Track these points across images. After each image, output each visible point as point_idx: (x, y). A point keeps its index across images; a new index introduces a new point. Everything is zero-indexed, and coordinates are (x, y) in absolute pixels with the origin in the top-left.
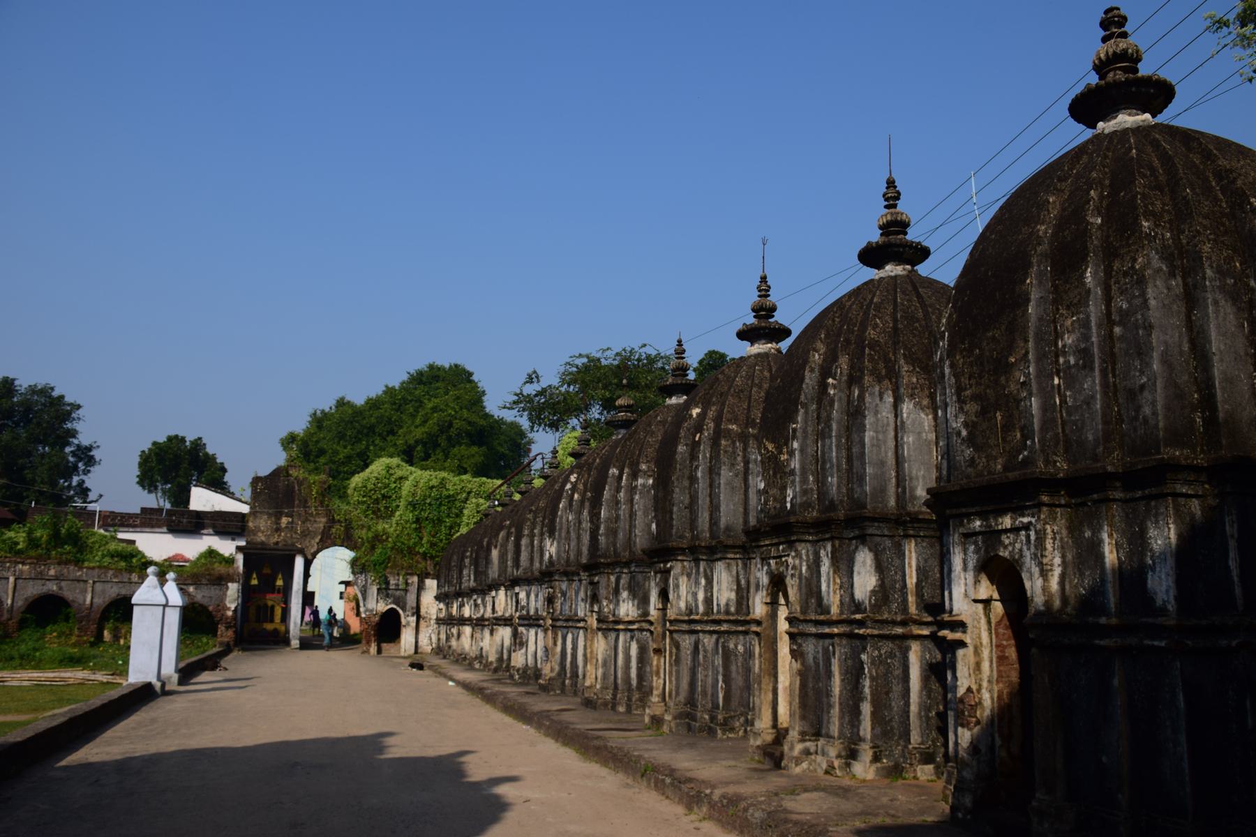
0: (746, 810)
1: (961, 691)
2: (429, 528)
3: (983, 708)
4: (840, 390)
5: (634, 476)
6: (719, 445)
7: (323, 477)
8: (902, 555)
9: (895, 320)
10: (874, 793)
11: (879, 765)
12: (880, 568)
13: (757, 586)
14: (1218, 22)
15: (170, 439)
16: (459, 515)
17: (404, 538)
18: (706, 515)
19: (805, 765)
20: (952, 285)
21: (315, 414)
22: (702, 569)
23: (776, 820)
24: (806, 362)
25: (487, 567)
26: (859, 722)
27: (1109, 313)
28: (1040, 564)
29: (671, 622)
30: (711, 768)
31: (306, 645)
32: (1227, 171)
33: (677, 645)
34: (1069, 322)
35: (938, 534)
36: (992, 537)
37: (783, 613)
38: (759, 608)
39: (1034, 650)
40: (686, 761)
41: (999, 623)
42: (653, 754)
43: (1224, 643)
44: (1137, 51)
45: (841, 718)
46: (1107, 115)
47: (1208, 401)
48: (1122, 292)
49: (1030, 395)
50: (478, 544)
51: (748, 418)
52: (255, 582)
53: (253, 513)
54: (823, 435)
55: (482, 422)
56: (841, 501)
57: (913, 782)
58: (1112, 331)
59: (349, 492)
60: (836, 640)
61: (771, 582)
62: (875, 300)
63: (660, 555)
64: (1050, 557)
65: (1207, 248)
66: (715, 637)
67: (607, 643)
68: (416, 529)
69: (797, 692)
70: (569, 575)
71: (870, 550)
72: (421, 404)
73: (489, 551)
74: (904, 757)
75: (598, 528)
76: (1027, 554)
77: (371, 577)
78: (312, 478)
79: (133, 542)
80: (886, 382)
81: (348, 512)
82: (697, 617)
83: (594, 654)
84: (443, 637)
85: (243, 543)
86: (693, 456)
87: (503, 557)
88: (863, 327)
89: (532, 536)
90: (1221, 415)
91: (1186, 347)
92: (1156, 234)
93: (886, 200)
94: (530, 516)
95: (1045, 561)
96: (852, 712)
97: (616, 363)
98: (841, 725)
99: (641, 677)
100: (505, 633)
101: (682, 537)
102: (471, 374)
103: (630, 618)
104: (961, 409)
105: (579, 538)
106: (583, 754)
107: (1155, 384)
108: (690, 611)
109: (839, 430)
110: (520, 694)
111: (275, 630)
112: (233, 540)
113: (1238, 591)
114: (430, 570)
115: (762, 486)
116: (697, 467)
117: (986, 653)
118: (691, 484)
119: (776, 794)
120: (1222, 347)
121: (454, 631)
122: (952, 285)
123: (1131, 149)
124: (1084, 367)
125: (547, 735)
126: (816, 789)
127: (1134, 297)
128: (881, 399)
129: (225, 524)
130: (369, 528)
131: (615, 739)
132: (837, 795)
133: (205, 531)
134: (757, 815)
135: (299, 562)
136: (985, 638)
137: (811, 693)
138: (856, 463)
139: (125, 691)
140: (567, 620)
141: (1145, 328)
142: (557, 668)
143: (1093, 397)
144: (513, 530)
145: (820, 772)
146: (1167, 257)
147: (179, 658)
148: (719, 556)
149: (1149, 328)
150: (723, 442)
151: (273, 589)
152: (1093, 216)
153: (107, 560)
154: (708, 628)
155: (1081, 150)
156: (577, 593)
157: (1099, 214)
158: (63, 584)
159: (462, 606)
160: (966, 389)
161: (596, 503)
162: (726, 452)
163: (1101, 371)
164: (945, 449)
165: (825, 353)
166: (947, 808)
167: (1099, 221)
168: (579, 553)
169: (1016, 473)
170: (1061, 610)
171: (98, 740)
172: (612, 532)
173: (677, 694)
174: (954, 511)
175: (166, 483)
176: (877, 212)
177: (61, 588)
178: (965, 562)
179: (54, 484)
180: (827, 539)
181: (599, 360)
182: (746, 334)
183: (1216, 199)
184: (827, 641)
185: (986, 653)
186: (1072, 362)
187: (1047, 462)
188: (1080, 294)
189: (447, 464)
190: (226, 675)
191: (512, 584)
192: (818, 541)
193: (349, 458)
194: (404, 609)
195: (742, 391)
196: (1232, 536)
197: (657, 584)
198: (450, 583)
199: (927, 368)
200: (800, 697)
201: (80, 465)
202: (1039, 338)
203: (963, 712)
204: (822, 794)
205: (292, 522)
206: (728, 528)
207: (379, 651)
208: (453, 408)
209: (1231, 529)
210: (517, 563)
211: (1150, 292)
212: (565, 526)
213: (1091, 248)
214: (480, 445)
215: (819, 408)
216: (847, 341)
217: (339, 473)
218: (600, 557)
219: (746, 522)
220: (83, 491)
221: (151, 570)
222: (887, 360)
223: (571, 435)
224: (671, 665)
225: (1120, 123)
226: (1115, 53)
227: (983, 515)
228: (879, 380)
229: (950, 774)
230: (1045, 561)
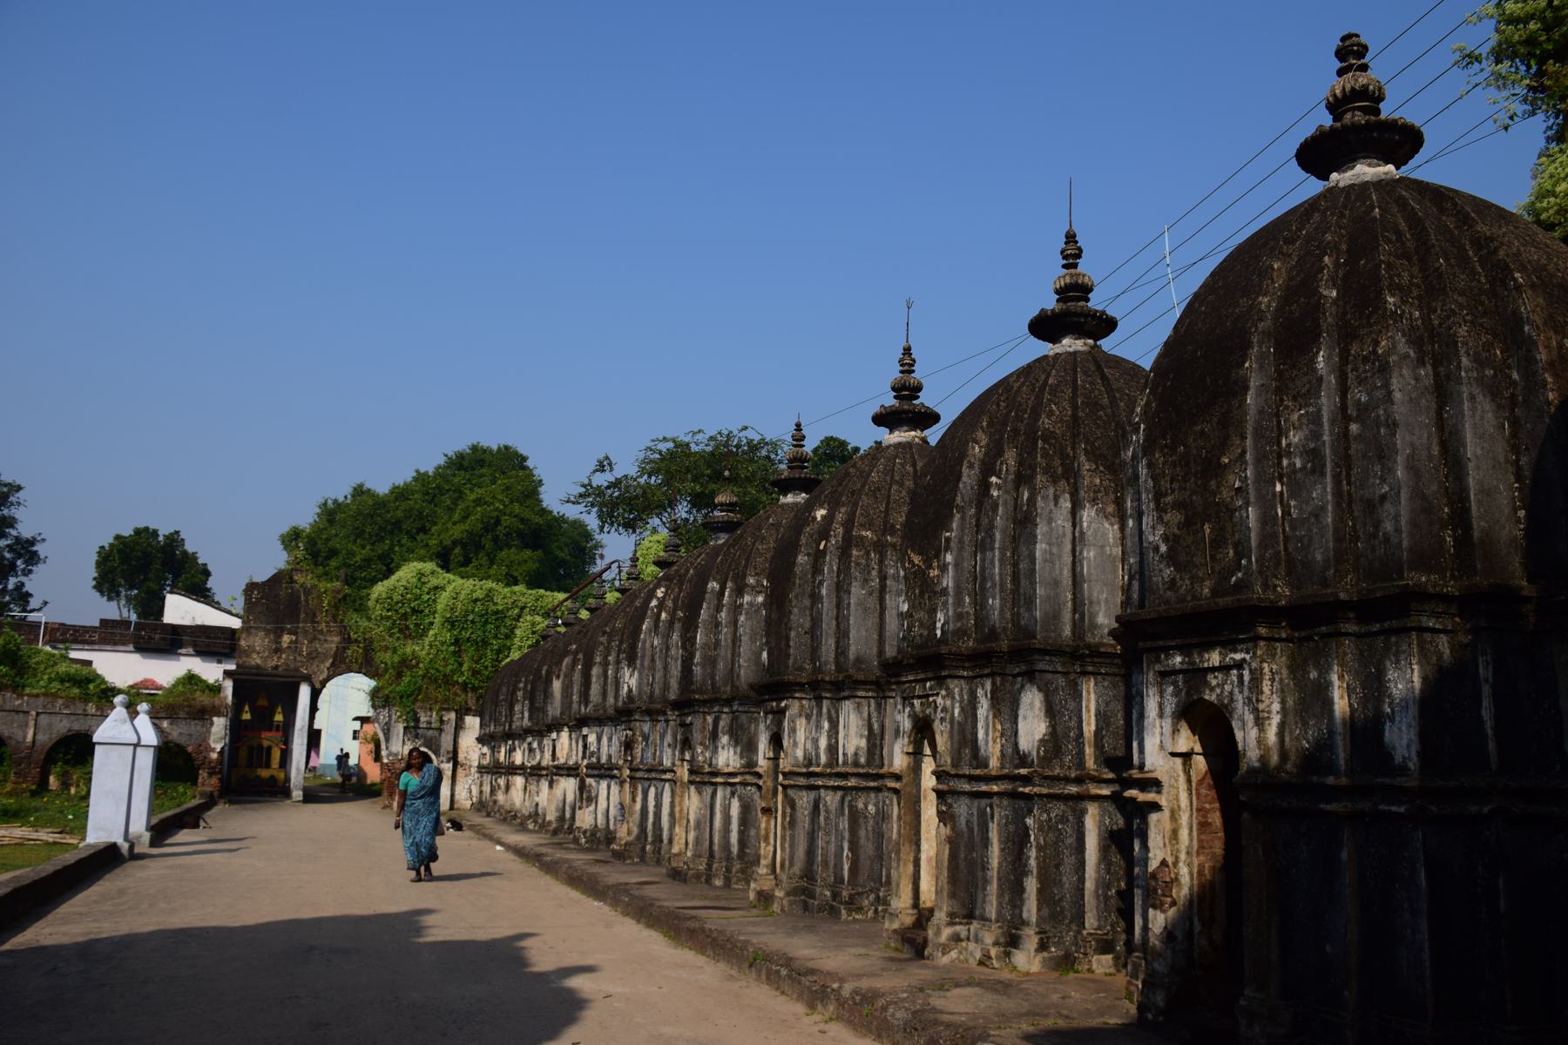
0: (884, 1008)
1: (1153, 865)
2: (471, 651)
4: (1006, 492)
5: (739, 591)
6: (850, 556)
8: (1077, 696)
9: (1062, 409)
10: (1040, 989)
11: (1045, 954)
12: (1051, 712)
13: (897, 733)
14: (1468, 56)
15: (138, 532)
16: (510, 636)
17: (439, 664)
18: (832, 642)
19: (954, 954)
20: (1147, 363)
21: (325, 504)
23: (923, 1021)
24: (963, 455)
25: (545, 702)
26: (1022, 901)
27: (1344, 407)
28: (1256, 711)
29: (785, 774)
31: (311, 797)
32: (1486, 238)
33: (791, 803)
34: (1295, 417)
36: (1196, 676)
37: (928, 766)
38: (898, 759)
39: (1245, 815)
40: (805, 948)
41: (1200, 782)
42: (764, 939)
43: (1474, 809)
44: (1380, 89)
45: (1000, 895)
46: (1342, 164)
47: (1461, 517)
49: (1247, 504)
51: (886, 522)
52: (247, 716)
53: (246, 629)
54: (983, 546)
55: (537, 519)
56: (1005, 629)
58: (1347, 428)
59: (371, 604)
60: (996, 800)
63: (772, 691)
64: (1267, 702)
65: (1462, 331)
66: (840, 794)
67: (702, 801)
68: (454, 653)
69: (946, 864)
70: (652, 714)
71: (1040, 690)
72: (460, 495)
73: (549, 682)
75: (692, 656)
76: (1239, 698)
78: (323, 586)
80: (1063, 482)
81: (367, 630)
83: (685, 814)
84: (487, 789)
85: (233, 667)
86: (817, 569)
87: (567, 689)
88: (1036, 416)
89: (605, 664)
90: (1476, 534)
91: (1436, 451)
94: (603, 639)
95: (1261, 706)
96: (1013, 889)
97: (709, 449)
98: (1000, 904)
99: (743, 842)
100: (568, 786)
101: (801, 669)
102: (524, 459)
103: (730, 770)
104: (1160, 519)
105: (666, 668)
108: (809, 762)
109: (1003, 541)
110: (588, 862)
112: (219, 662)
113: (1492, 746)
114: (472, 703)
115: (905, 607)
116: (821, 583)
117: (1184, 819)
118: (813, 604)
119: (921, 990)
120: (1479, 452)
121: (502, 781)
122: (1147, 363)
123: (1372, 208)
124: (1313, 471)
125: (627, 914)
127: (1376, 388)
128: (1056, 504)
129: (209, 642)
130: (395, 651)
131: (714, 920)
132: (996, 991)
133: (183, 651)
134: (898, 1015)
135: (304, 692)
137: (962, 864)
138: (1023, 582)
142: (635, 830)
143: (1323, 508)
144: (580, 656)
145: (973, 963)
146: (1416, 341)
148: (846, 693)
149: (1393, 426)
151: (270, 726)
152: (1327, 287)
153: (56, 685)
156: (662, 738)
157: (1334, 286)
159: (512, 750)
160: (1166, 495)
161: (690, 626)
162: (858, 564)
164: (1135, 568)
165: (988, 445)
166: (1133, 1010)
167: (1334, 294)
168: (666, 686)
169: (1228, 599)
170: (1279, 768)
171: (50, 917)
172: (710, 662)
173: (791, 864)
174: (1149, 644)
175: (131, 588)
176: (1053, 273)
180: (987, 676)
181: (688, 445)
182: (884, 419)
183: (1473, 272)
184: (984, 802)
185: (1184, 819)
186: (1298, 465)
187: (1266, 586)
188: (1309, 382)
189: (492, 572)
190: (211, 834)
193: (368, 561)
194: (437, 754)
195: (878, 489)
196: (1487, 681)
197: (767, 728)
198: (497, 722)
199: (1109, 461)
200: (949, 870)
201: (19, 562)
202: (1259, 433)
203: (1155, 891)
205: (296, 642)
206: (859, 660)
208: (502, 501)
209: (1485, 671)
211: (1395, 383)
212: (648, 653)
214: (535, 547)
215: (979, 512)
216: (1015, 431)
217: (355, 580)
219: (881, 652)
220: (23, 597)
221: (118, 699)
222: (1064, 457)
223: (655, 537)
224: (783, 828)
225: (1358, 175)
227: (1185, 650)
229: (1136, 967)
230: (1261, 706)
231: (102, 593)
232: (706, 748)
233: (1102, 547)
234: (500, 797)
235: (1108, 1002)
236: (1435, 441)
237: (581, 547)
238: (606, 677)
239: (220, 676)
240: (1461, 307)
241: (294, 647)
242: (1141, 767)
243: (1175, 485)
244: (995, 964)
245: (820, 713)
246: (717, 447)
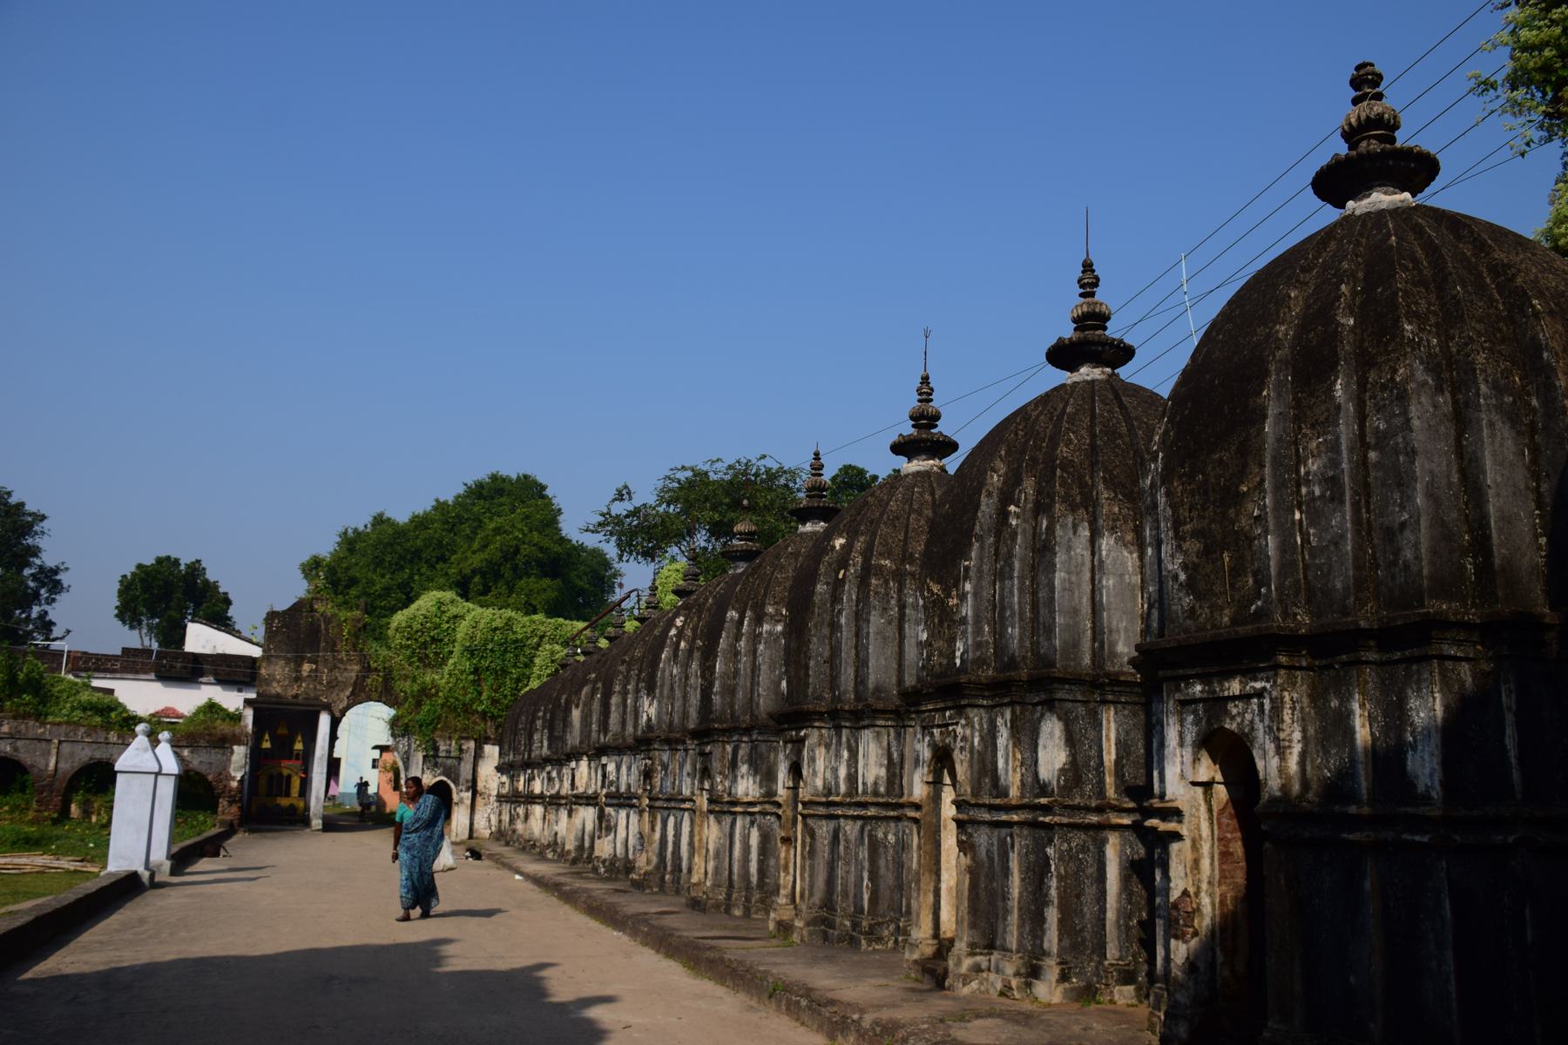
1: (1175, 895)
3: (1201, 915)
4: (1025, 521)
5: (759, 620)
6: (869, 585)
8: (1098, 725)
9: (1081, 435)
10: (1062, 1020)
11: (1067, 985)
12: (1071, 741)
13: (917, 762)
14: (1484, 83)
15: (160, 561)
16: (529, 664)
18: (851, 671)
19: (974, 985)
20: (1165, 391)
21: (345, 533)
22: (844, 739)
24: (982, 484)
25: (564, 731)
26: (1043, 932)
28: (1277, 740)
29: (804, 804)
30: (861, 988)
31: (330, 825)
32: (1504, 265)
35: (1143, 700)
36: (1217, 705)
37: (948, 795)
38: (918, 789)
39: (1267, 845)
40: (824, 978)
41: (1221, 812)
44: (1395, 117)
46: (1359, 192)
47: (1481, 544)
49: (1266, 532)
50: (553, 703)
51: (904, 551)
52: (267, 745)
53: (267, 657)
54: (1002, 575)
55: (557, 549)
56: (1024, 658)
57: (1110, 1007)
58: (1365, 457)
60: (1016, 830)
61: (934, 756)
62: (1069, 410)
63: (791, 720)
64: (1288, 731)
65: (1481, 358)
66: (859, 823)
67: (721, 829)
68: (473, 682)
69: (966, 893)
70: (672, 743)
71: (1060, 719)
73: (568, 711)
74: (1098, 975)
75: (711, 684)
76: (1260, 727)
77: (415, 741)
78: (344, 614)
80: (1081, 511)
82: (837, 799)
83: (705, 844)
84: (506, 818)
85: (253, 696)
86: (836, 598)
87: (586, 719)
88: (1054, 443)
89: (624, 693)
90: (1497, 561)
91: (1455, 478)
94: (622, 668)
95: (1282, 735)
96: (1034, 919)
97: (727, 478)
98: (1021, 935)
99: (762, 872)
100: (587, 815)
101: (820, 698)
102: (543, 488)
103: (750, 799)
104: (1179, 547)
105: (685, 697)
106: (693, 969)
107: (1418, 522)
108: (828, 791)
109: (1022, 569)
110: (607, 892)
112: (240, 691)
113: (1516, 775)
114: (491, 732)
115: (924, 636)
116: (840, 612)
117: (1206, 848)
118: (832, 633)
119: (942, 1021)
120: (1499, 479)
121: (521, 810)
122: (1165, 391)
123: (1389, 236)
124: (1332, 499)
125: (645, 944)
126: (990, 1015)
130: (414, 680)
131: (734, 950)
132: (1018, 1022)
133: (204, 679)
135: (324, 721)
136: (1205, 826)
137: (983, 894)
138: (1043, 611)
139: (104, 883)
140: (668, 800)
141: (1407, 454)
142: (655, 860)
143: (1342, 536)
144: (600, 685)
145: (994, 994)
146: (1433, 367)
148: (866, 722)
149: (1412, 454)
151: (290, 754)
152: (1344, 315)
153: (78, 713)
154: (851, 813)
155: (1324, 238)
156: (681, 767)
157: (1352, 314)
158: (19, 743)
159: (531, 779)
161: (709, 655)
162: (877, 593)
163: (1353, 504)
164: (1155, 596)
165: (1006, 474)
167: (1352, 322)
168: (685, 715)
169: (1249, 628)
170: (1301, 796)
171: (72, 945)
172: (730, 691)
173: (811, 894)
174: (1169, 673)
175: (153, 617)
177: (16, 749)
180: (1006, 705)
181: (706, 473)
182: (903, 448)
183: (1491, 298)
184: (1004, 831)
185: (1206, 848)
186: (1317, 492)
187: (1285, 614)
188: (1327, 410)
189: (511, 600)
191: (597, 753)
192: (993, 707)
194: (456, 783)
196: (1509, 708)
197: (787, 757)
198: (516, 750)
199: (1129, 492)
204: (998, 1021)
205: (316, 670)
206: (878, 689)
208: (521, 530)
209: (1508, 700)
211: (1414, 411)
212: (667, 683)
213: (1342, 354)
214: (554, 576)
215: (997, 542)
216: (1034, 460)
218: (714, 721)
219: (900, 681)
220: (46, 626)
221: (140, 728)
222: (1082, 485)
223: (674, 565)
225: (1374, 203)
226: (1368, 118)
227: (1205, 679)
228: (1073, 508)
229: (1158, 998)
230: (1282, 735)
231: (124, 622)
232: (726, 777)
233: (1122, 575)
236: (1455, 468)
237: (600, 575)
238: (625, 706)
239: (241, 704)
241: (315, 676)
242: (1162, 796)
243: (1195, 514)
245: (839, 742)
246: (736, 475)
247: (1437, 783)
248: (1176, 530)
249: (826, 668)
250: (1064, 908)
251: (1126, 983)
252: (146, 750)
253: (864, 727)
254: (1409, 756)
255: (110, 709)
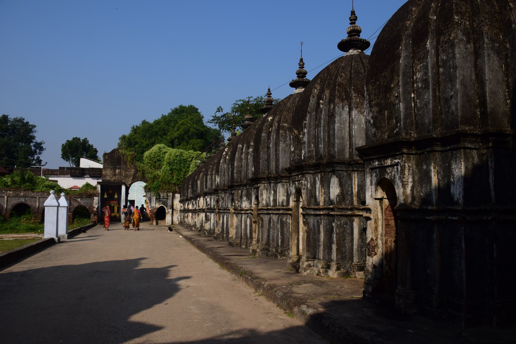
0: (276, 292)
1: (369, 240)
4: (325, 106)
5: (248, 148)
6: (279, 133)
7: (133, 153)
10: (334, 284)
11: (339, 271)
12: (341, 185)
15: (74, 139)
17: (166, 177)
18: (274, 163)
19: (308, 271)
21: (133, 127)
22: (272, 187)
24: (311, 93)
26: (331, 253)
27: (437, 62)
28: (402, 182)
30: (266, 272)
36: (383, 169)
38: (292, 204)
41: (386, 209)
45: (324, 251)
47: (483, 104)
48: (444, 51)
49: (400, 102)
52: (106, 196)
53: (104, 168)
54: (318, 126)
55: (202, 129)
56: (325, 155)
57: (355, 279)
58: (439, 70)
59: (144, 158)
60: (322, 217)
63: (255, 181)
64: (407, 178)
65: (486, 28)
66: (277, 216)
68: (171, 173)
69: (305, 240)
70: (224, 191)
71: (337, 177)
74: (351, 268)
75: (233, 170)
76: (397, 177)
77: (153, 193)
79: (57, 181)
80: (346, 101)
82: (270, 208)
85: (101, 181)
86: (269, 138)
87: (202, 184)
89: (212, 175)
90: (489, 110)
91: (474, 77)
92: (462, 22)
93: (350, 20)
94: (211, 166)
95: (404, 180)
96: (329, 249)
98: (324, 254)
100: (203, 215)
101: (264, 173)
102: (197, 109)
103: (247, 208)
104: (371, 110)
108: (268, 205)
109: (324, 123)
110: (205, 241)
111: (115, 216)
113: (493, 193)
114: (177, 190)
116: (270, 143)
117: (380, 223)
119: (291, 285)
120: (491, 77)
121: (186, 215)
125: (210, 258)
127: (450, 53)
128: (343, 109)
129: (93, 173)
130: (152, 173)
131: (234, 260)
132: (318, 285)
133: (86, 176)
134: (280, 294)
135: (123, 188)
136: (380, 215)
137: (311, 240)
138: (332, 138)
141: (454, 68)
142: (220, 230)
143: (428, 102)
145: (315, 274)
146: (466, 33)
147: (67, 229)
148: (279, 181)
149: (455, 68)
150: (281, 131)
151: (113, 199)
152: (432, 15)
153: (45, 188)
154: (275, 212)
157: (435, 14)
158: (27, 199)
159: (188, 204)
162: (282, 136)
167: (435, 18)
171: (22, 262)
172: (239, 172)
173: (262, 240)
175: (73, 157)
176: (347, 26)
177: (26, 201)
178: (371, 181)
179: (26, 158)
180: (319, 172)
184: (319, 218)
185: (380, 223)
186: (420, 86)
187: (407, 133)
188: (424, 53)
189: (188, 147)
192: (315, 173)
194: (167, 206)
195: (290, 109)
198: (184, 195)
202: (405, 74)
204: (311, 284)
207: (157, 224)
208: (190, 124)
210: (206, 187)
211: (457, 50)
212: (223, 170)
214: (201, 138)
215: (316, 114)
216: (329, 84)
218: (234, 182)
220: (39, 161)
222: (346, 92)
227: (379, 159)
228: (342, 100)
230: (404, 180)
232: (239, 201)
233: (360, 124)
234: (186, 220)
235: (357, 289)
236: (473, 74)
237: (217, 138)
238: (212, 179)
239: (96, 184)
240: (486, 19)
241: (120, 174)
243: (376, 97)
244: (322, 275)
245: (270, 188)
246: (258, 102)
247: (461, 197)
248: (370, 103)
249: (266, 162)
250: (338, 245)
251: (360, 271)
252: (53, 199)
253: (279, 183)
254: (452, 187)
255: (55, 187)
